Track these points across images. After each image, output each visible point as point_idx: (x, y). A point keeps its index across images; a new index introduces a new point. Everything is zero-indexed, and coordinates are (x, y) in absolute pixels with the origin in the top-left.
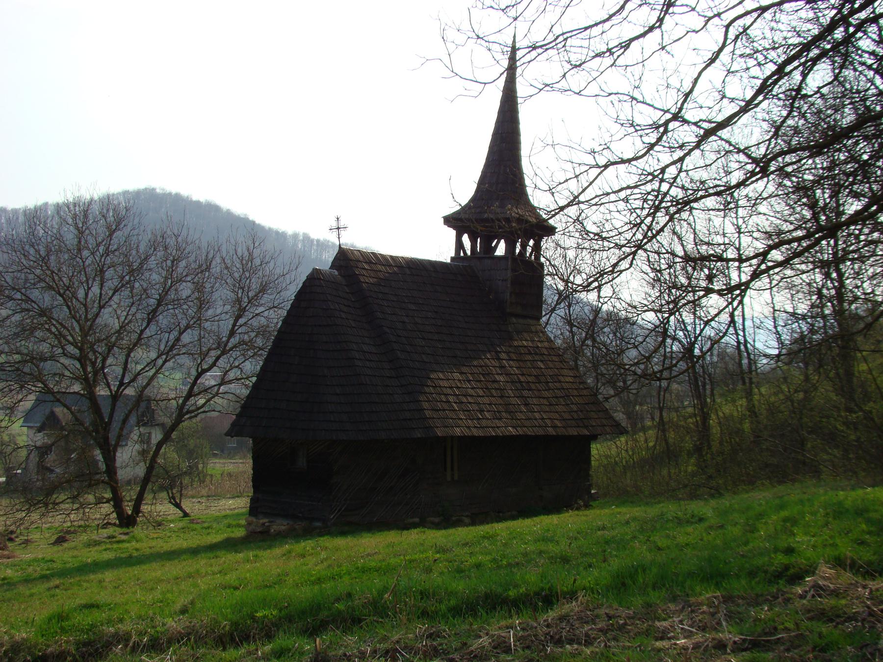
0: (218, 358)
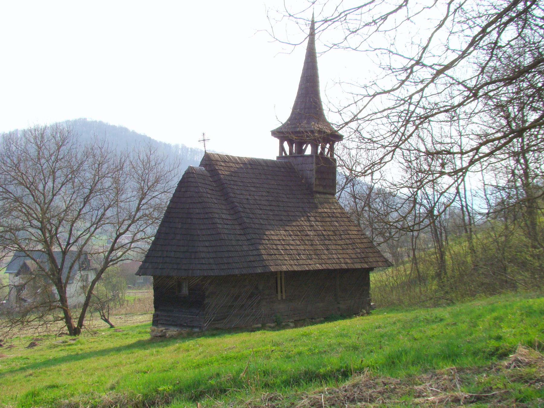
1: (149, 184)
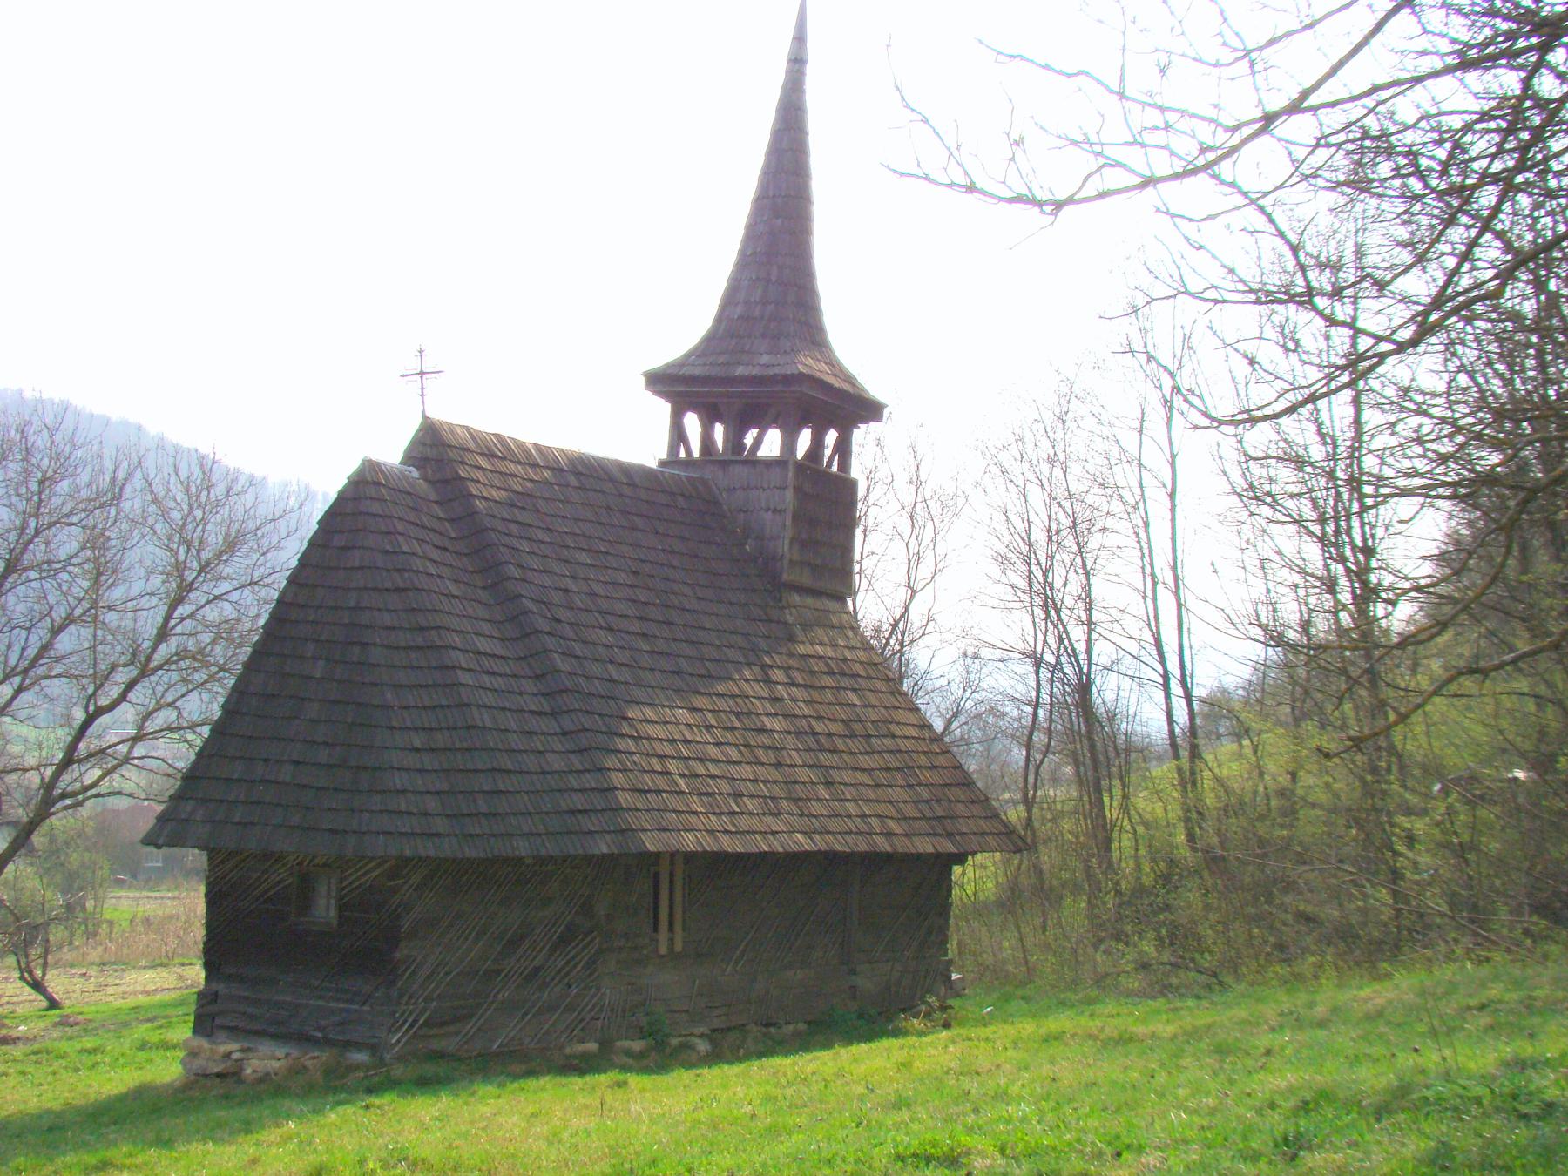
0: (131, 685)
1: (205, 555)
